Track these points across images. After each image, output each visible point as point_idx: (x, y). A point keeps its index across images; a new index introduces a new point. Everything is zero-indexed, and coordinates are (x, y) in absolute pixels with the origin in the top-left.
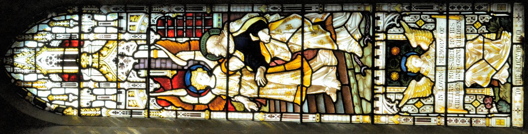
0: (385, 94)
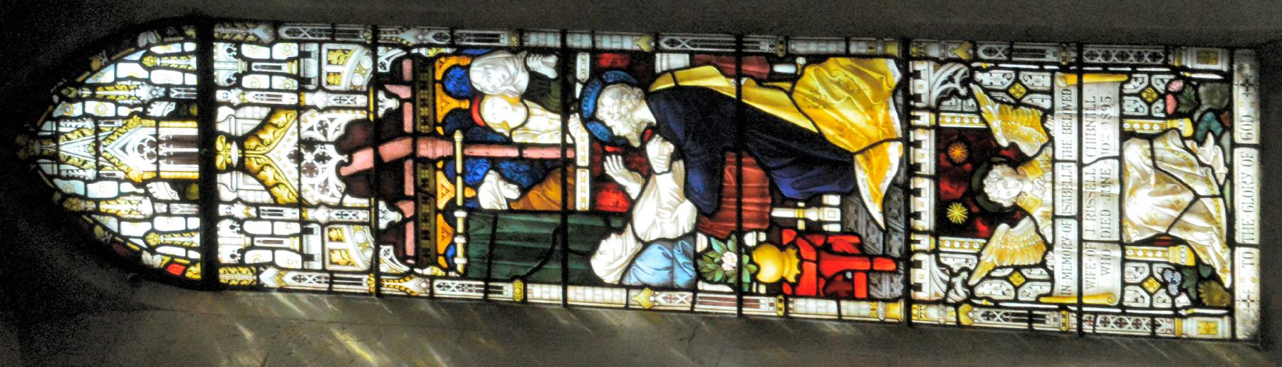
0: (936, 252)
